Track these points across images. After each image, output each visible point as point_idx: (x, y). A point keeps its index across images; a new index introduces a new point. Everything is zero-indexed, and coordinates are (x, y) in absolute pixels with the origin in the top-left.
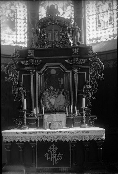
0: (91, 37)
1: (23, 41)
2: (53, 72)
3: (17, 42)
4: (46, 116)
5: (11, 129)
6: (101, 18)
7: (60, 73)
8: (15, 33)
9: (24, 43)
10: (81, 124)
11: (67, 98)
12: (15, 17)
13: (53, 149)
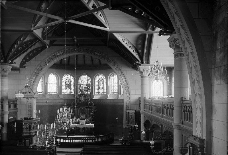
0: (97, 92)
1: (72, 92)
2: (82, 109)
3: (70, 93)
4: (80, 121)
5: (8, 57)
6: (100, 86)
7: (84, 109)
8: (70, 89)
9: (73, 93)
10: (89, 123)
11: (86, 116)
12: (70, 84)
13: (82, 129)
